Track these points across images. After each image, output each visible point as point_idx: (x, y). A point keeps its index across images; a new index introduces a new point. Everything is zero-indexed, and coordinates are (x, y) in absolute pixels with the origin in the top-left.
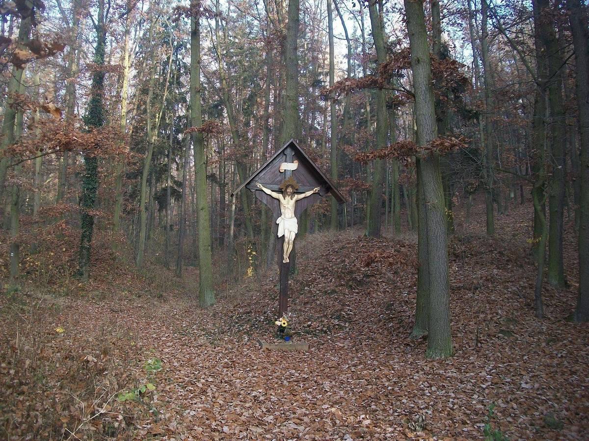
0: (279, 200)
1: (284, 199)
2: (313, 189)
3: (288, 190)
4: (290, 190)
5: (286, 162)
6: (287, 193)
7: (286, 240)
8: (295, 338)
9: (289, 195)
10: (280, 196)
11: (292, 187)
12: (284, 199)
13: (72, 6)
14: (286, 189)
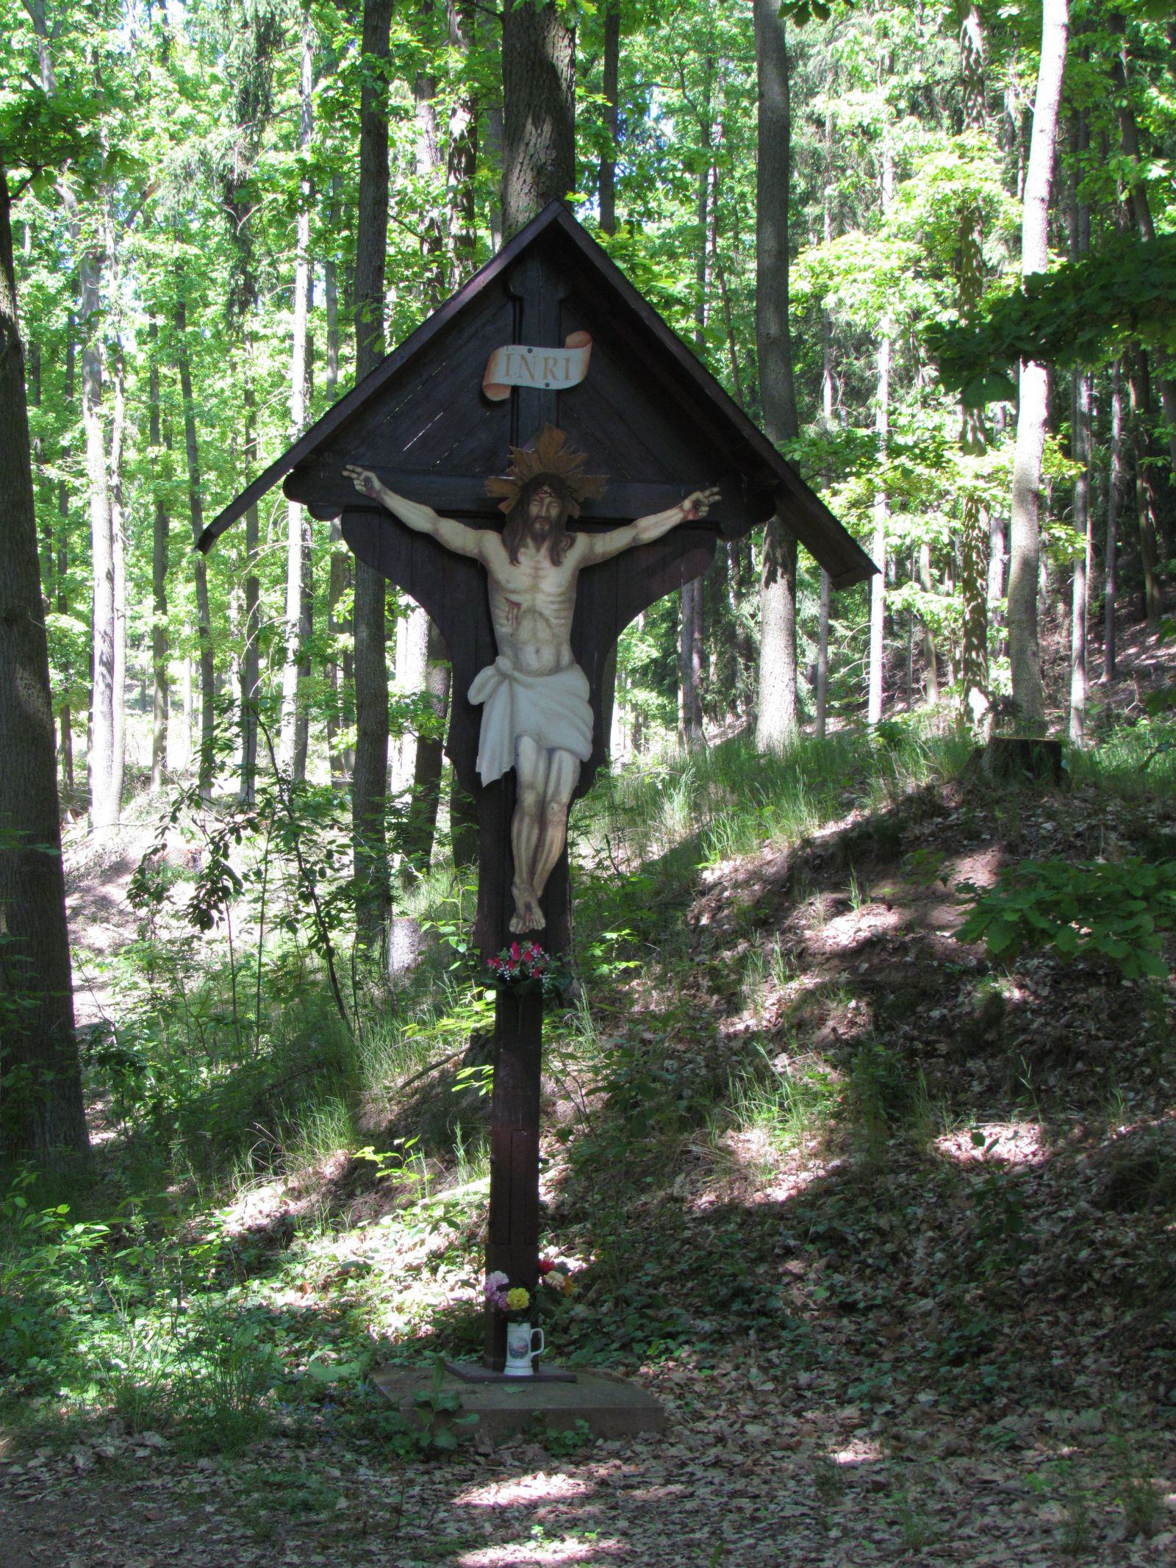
0: (478, 568)
1: (514, 560)
2: (675, 502)
3: (534, 510)
4: (544, 507)
5: (517, 339)
6: (528, 522)
7: (529, 799)
8: (289, 404)
9: (539, 540)
10: (490, 545)
11: (561, 488)
12: (514, 560)
13: (369, 1337)
14: (523, 503)
